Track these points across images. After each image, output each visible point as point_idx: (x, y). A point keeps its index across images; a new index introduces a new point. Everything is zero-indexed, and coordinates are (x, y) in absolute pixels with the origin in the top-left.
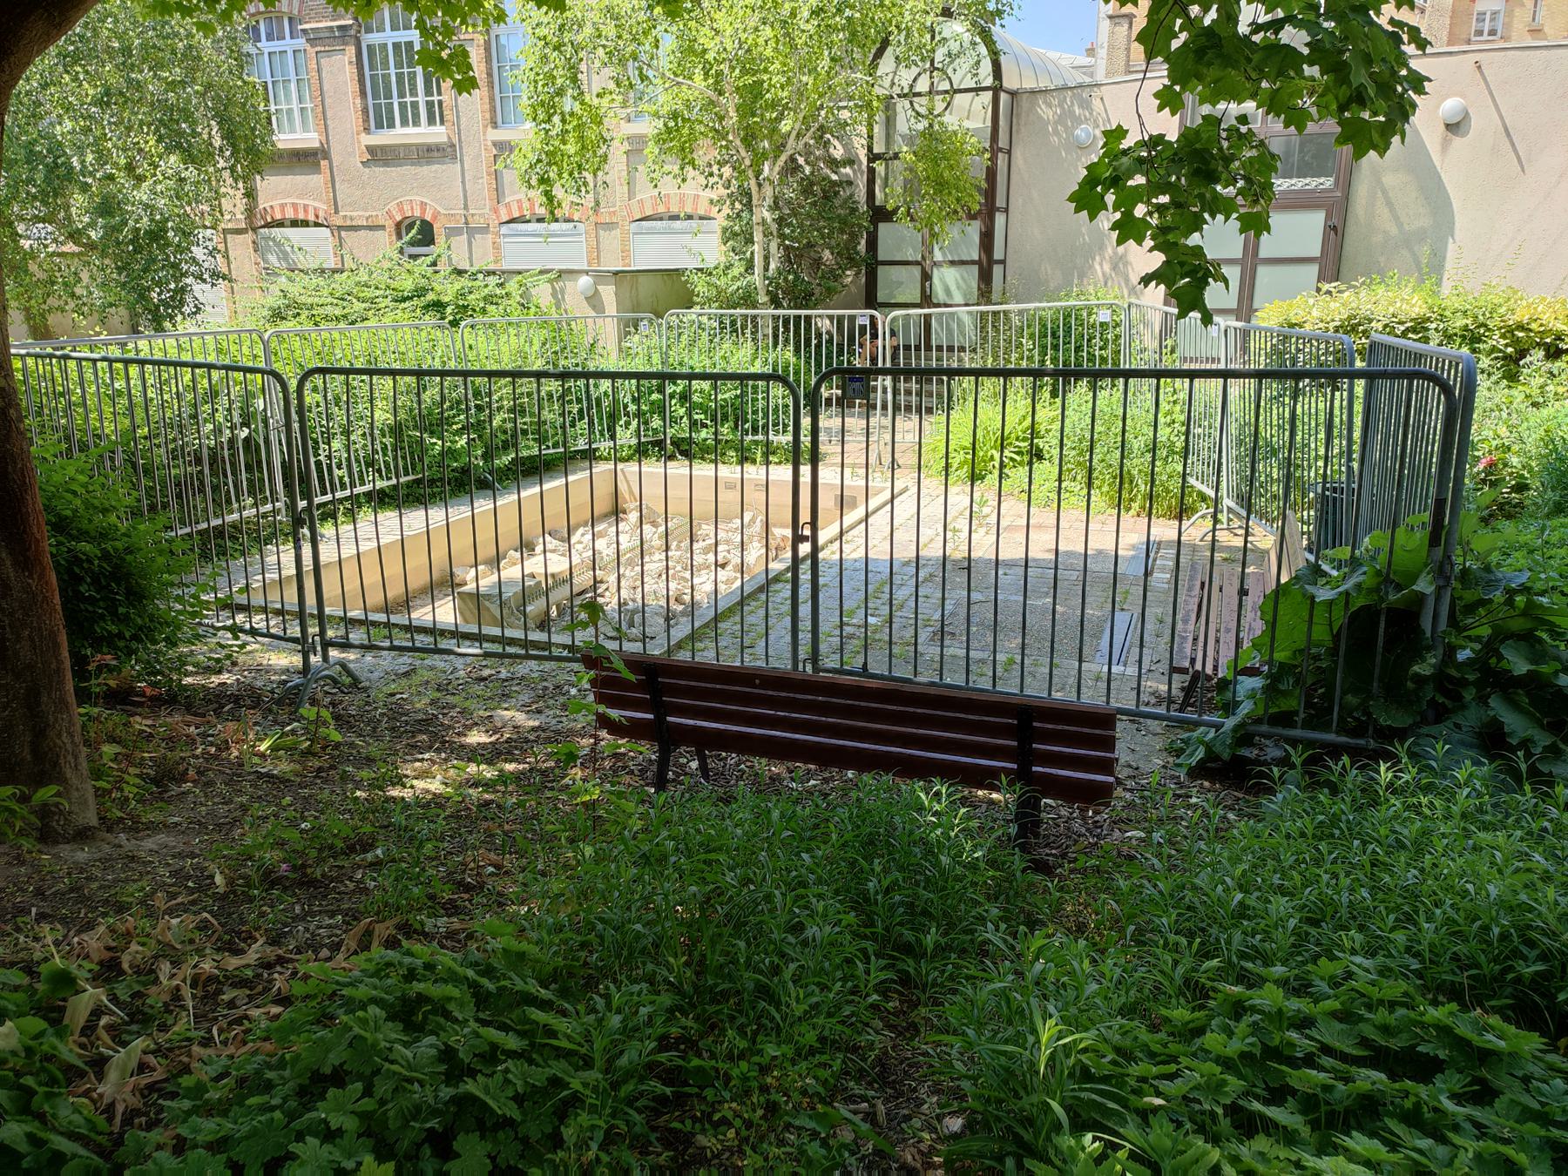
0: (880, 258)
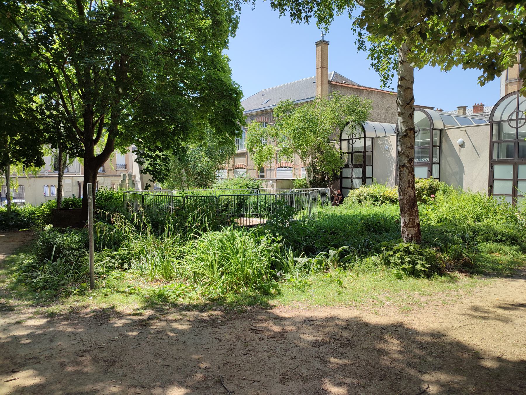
0: (366, 177)
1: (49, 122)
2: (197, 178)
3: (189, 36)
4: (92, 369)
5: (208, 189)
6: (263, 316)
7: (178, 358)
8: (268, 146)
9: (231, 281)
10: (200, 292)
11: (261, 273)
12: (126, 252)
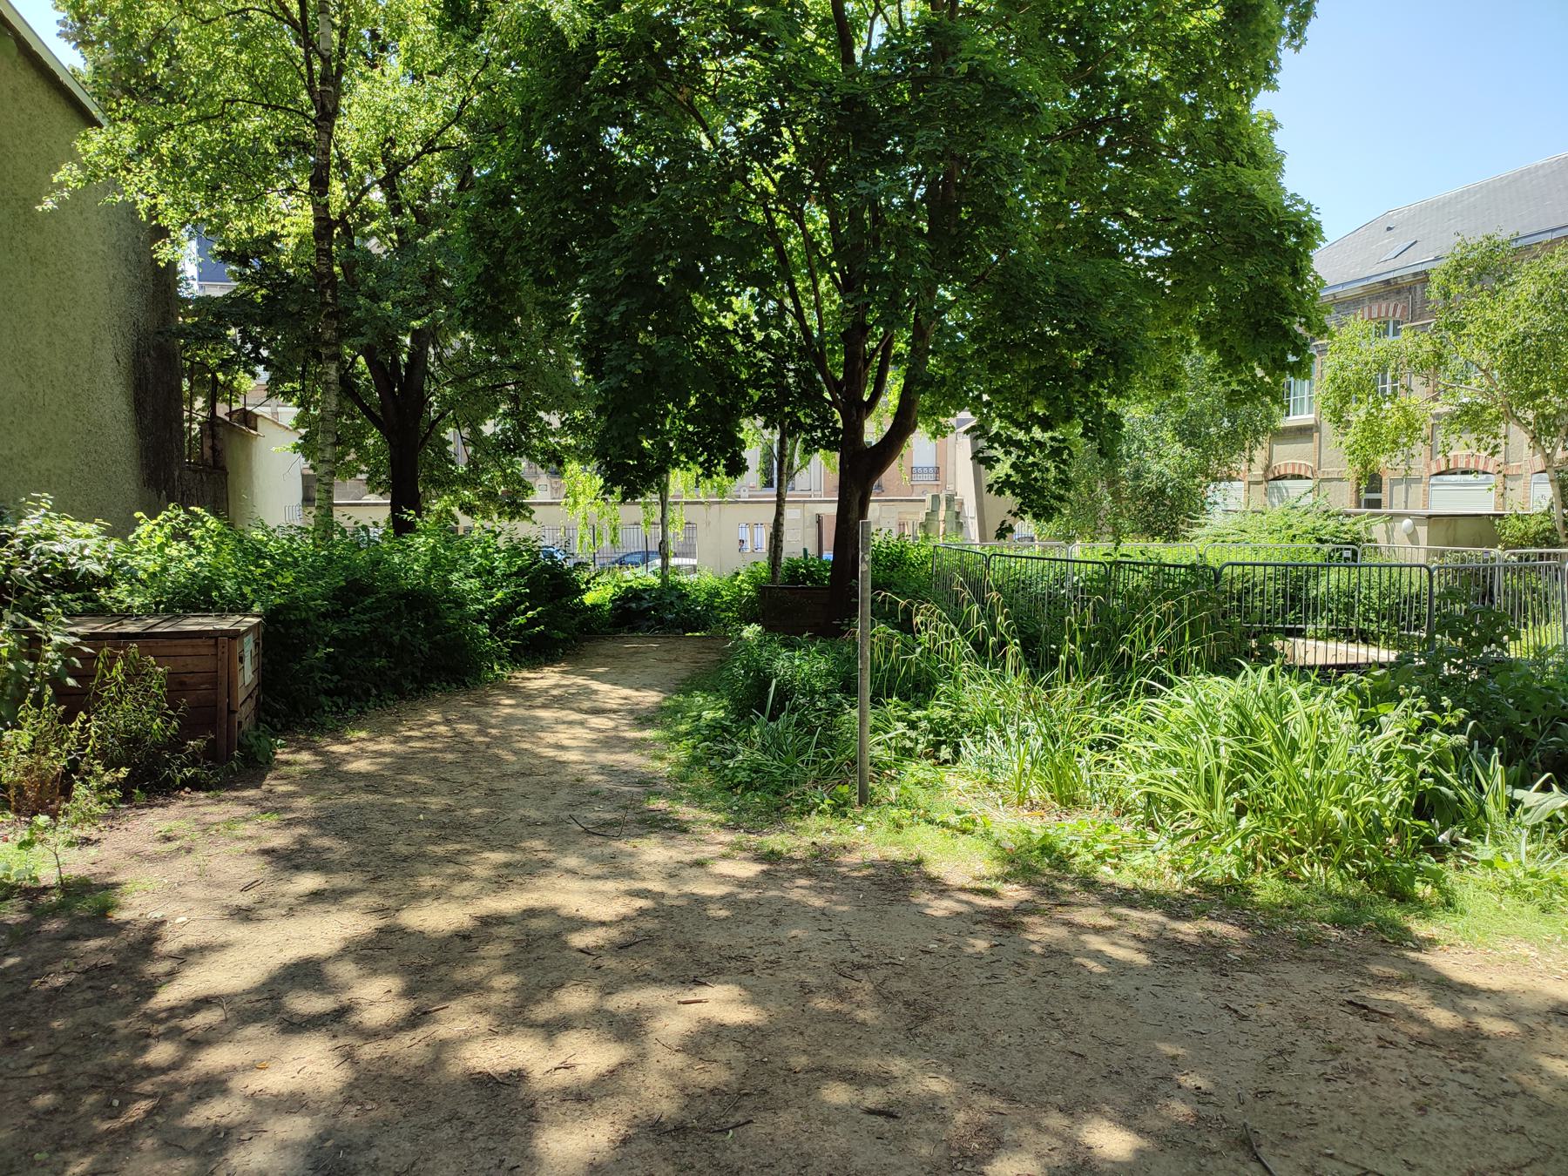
1: (761, 360)
2: (1145, 508)
3: (1145, 68)
4: (877, 1018)
5: (1181, 542)
6: (1388, 966)
7: (1108, 1039)
8: (1403, 399)
9: (1268, 837)
10: (1167, 857)
11: (1380, 827)
12: (947, 713)
